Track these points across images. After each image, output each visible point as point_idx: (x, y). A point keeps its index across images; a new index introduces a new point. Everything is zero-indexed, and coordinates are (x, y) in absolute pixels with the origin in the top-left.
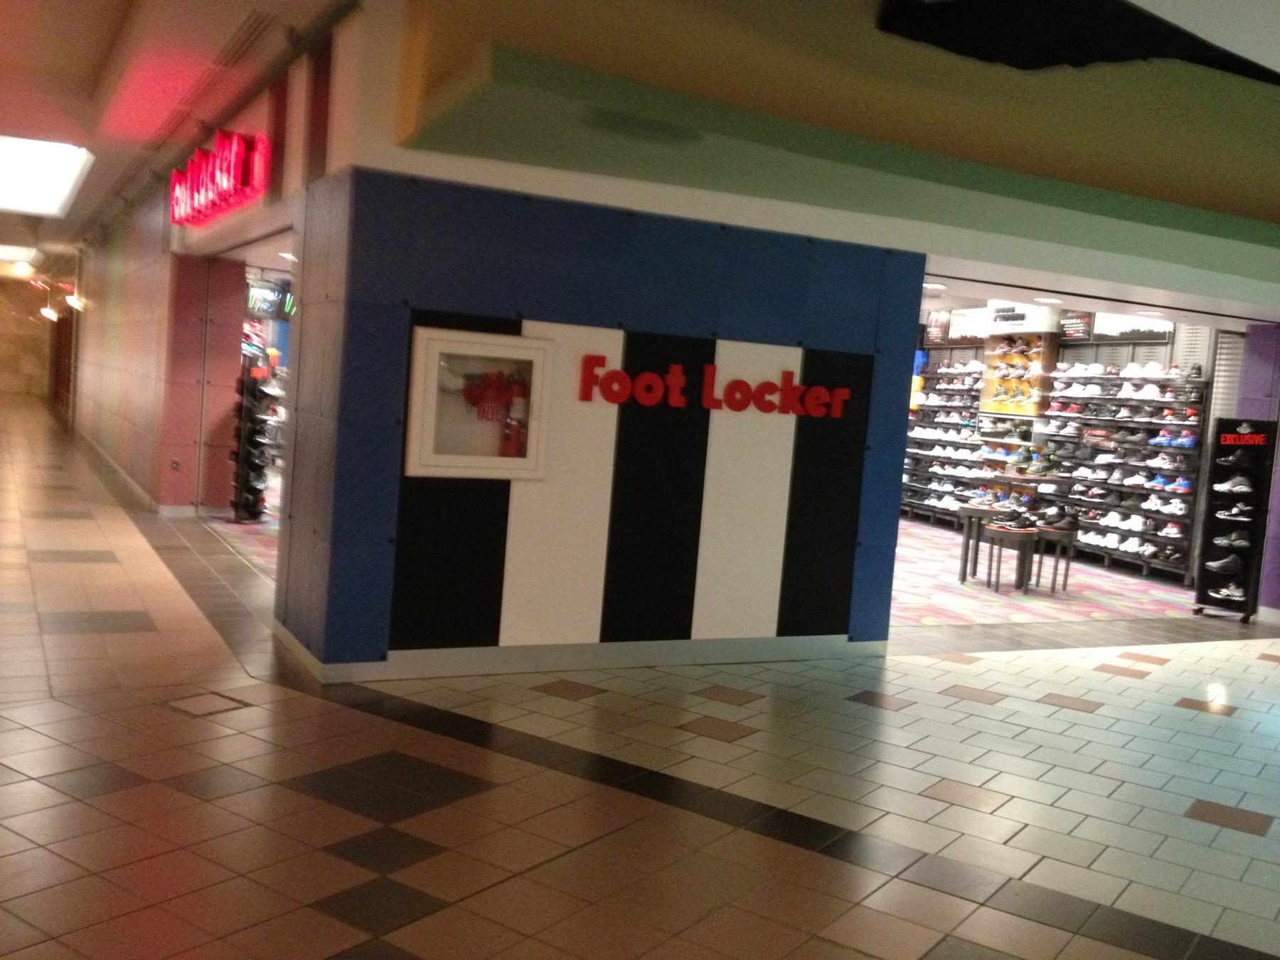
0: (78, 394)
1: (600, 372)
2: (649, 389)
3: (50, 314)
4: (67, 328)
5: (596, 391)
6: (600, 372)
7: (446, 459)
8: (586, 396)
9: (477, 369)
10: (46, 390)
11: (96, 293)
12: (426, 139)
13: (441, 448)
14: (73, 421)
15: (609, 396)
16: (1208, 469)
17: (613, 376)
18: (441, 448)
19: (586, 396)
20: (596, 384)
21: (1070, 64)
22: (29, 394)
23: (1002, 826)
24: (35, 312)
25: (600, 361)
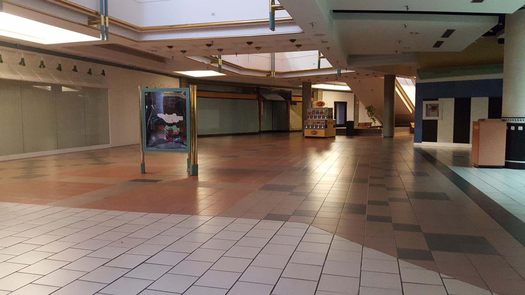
18: (427, 116)
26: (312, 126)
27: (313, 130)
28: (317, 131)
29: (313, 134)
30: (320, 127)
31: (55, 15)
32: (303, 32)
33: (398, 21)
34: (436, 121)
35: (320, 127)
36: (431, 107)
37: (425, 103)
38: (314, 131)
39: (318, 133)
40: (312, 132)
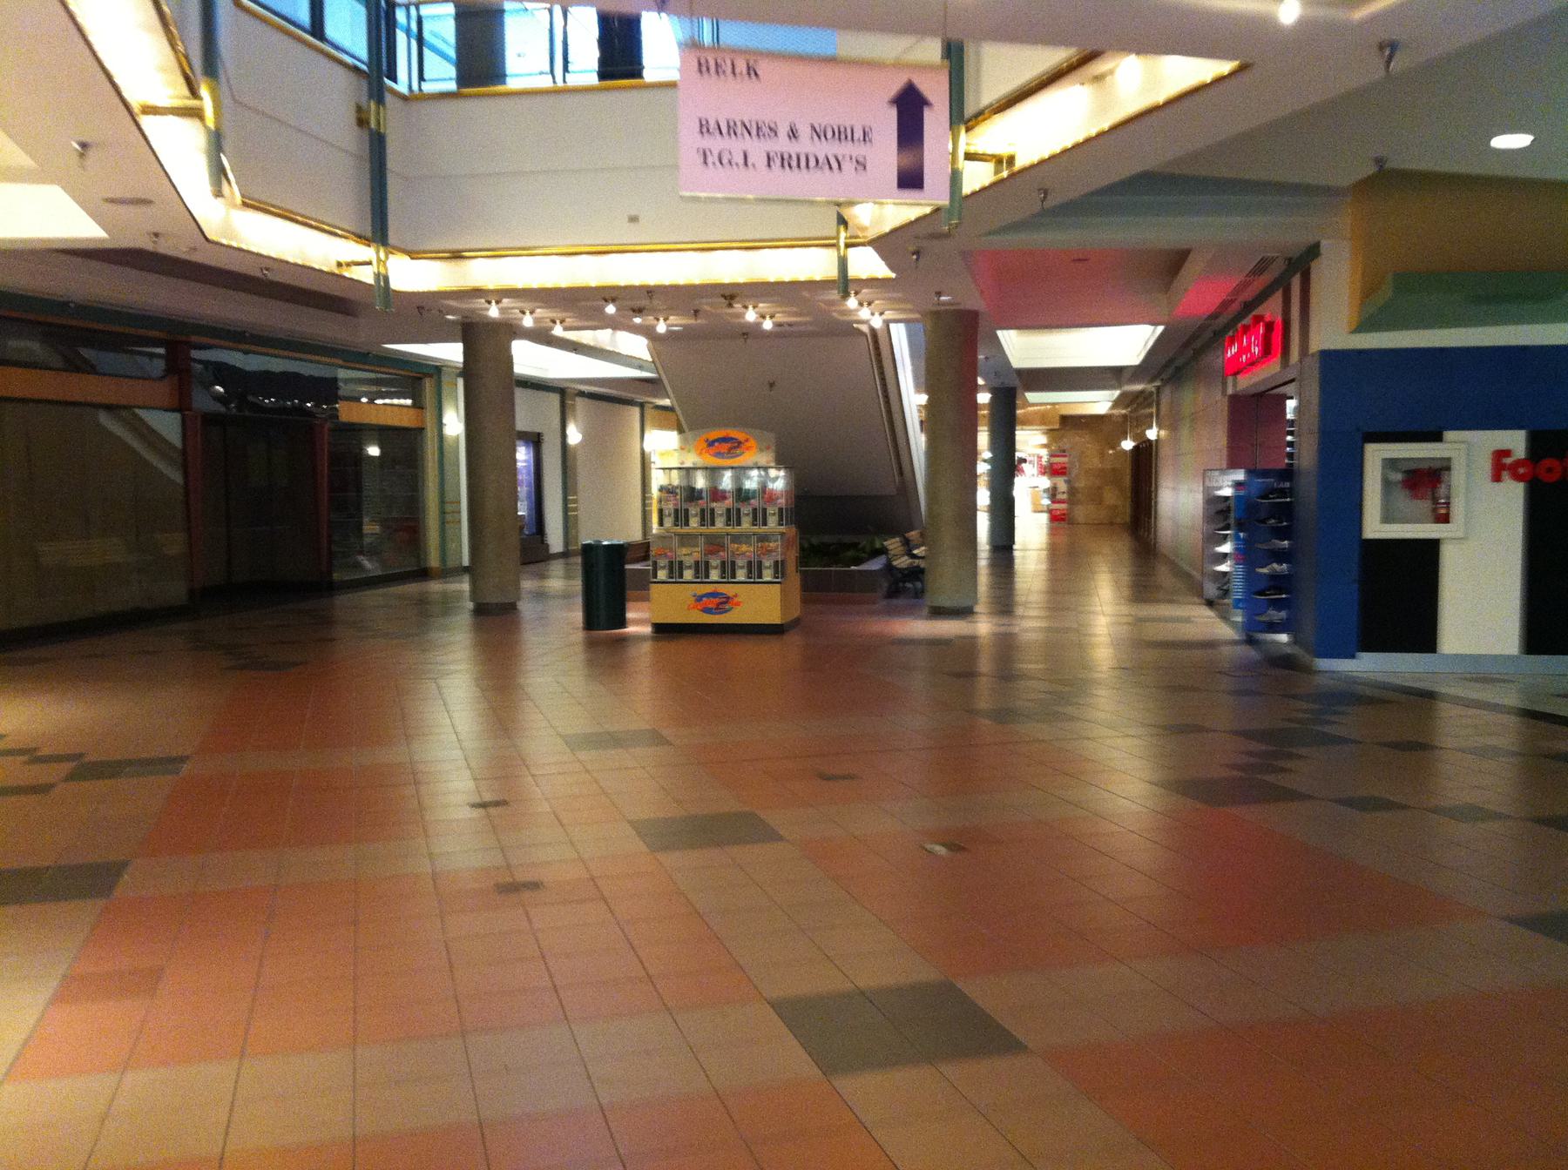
0: (1158, 518)
1: (1508, 461)
2: (1550, 470)
3: (1128, 445)
4: (1145, 457)
5: (1505, 474)
6: (1508, 461)
7: (1387, 527)
8: (1497, 478)
9: (1413, 466)
10: (1128, 519)
11: (1172, 424)
12: (1366, 324)
13: (1387, 518)
14: (1155, 544)
15: (1517, 477)
16: (430, 470)
17: (1519, 463)
18: (1387, 518)
19: (1497, 478)
20: (1504, 470)
21: (776, 457)
22: (1112, 524)
23: (1163, 569)
24: (1115, 444)
25: (1507, 453)
26: (702, 569)
27: (709, 588)
28: (730, 595)
29: (706, 610)
30: (755, 570)
31: (263, 198)
32: (1242, 69)
33: (430, 484)
34: (1428, 551)
35: (755, 570)
36: (752, 501)
37: (1376, 455)
38: (714, 595)
39: (738, 604)
40: (699, 598)
